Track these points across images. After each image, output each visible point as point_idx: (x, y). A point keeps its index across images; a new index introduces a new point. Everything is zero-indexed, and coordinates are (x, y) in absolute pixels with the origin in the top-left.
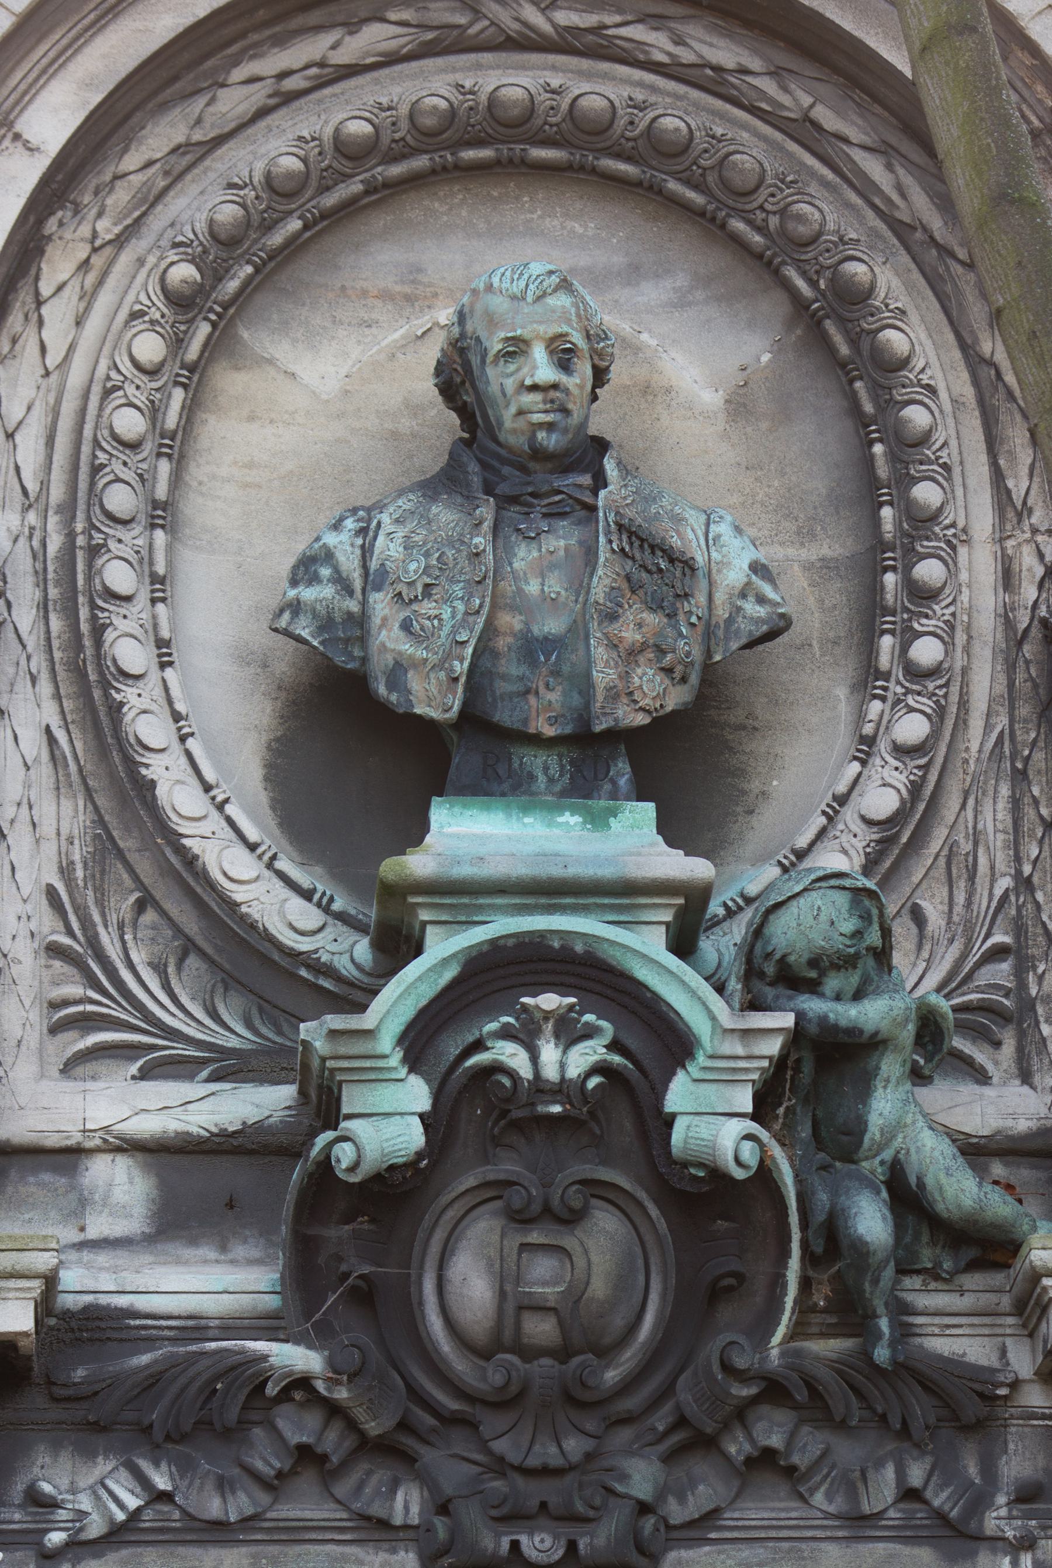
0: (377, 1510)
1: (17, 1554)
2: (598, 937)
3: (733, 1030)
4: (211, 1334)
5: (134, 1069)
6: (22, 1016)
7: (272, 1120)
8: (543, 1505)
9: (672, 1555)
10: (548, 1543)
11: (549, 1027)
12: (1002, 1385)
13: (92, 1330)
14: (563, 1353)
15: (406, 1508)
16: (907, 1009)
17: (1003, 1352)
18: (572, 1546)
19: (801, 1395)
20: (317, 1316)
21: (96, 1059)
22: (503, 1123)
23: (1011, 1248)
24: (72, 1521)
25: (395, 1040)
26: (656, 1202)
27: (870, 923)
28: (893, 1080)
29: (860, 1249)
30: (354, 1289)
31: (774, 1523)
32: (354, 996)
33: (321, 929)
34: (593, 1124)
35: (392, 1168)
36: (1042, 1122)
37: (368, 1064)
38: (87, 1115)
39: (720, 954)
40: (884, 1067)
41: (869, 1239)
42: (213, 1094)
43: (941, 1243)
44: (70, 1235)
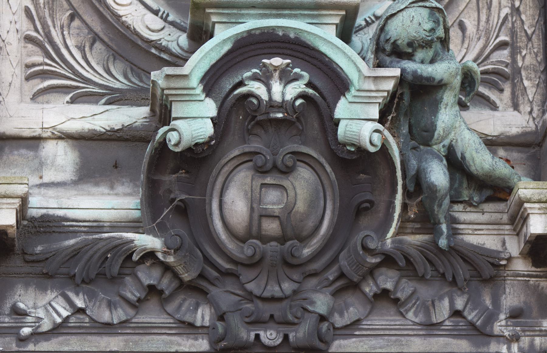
0: (188, 318)
1: (7, 339)
2: (302, 30)
3: (369, 77)
4: (105, 230)
5: (68, 98)
6: (12, 71)
7: (137, 124)
8: (272, 316)
9: (336, 343)
10: (274, 336)
11: (276, 75)
12: (503, 259)
13: (46, 227)
14: (282, 239)
15: (203, 318)
16: (457, 68)
17: (504, 243)
18: (286, 337)
19: (402, 263)
20: (159, 220)
21: (49, 93)
22: (253, 123)
23: (508, 191)
24: (35, 322)
25: (199, 80)
26: (330, 164)
27: (439, 25)
28: (450, 104)
29: (433, 189)
30: (177, 207)
31: (388, 327)
32: (180, 60)
33: (163, 29)
34: (298, 124)
35: (197, 145)
36: (524, 129)
37: (185, 92)
38: (44, 120)
39: (363, 44)
40: (445, 98)
41: (437, 184)
42: (107, 110)
43: (473, 188)
44: (34, 180)
